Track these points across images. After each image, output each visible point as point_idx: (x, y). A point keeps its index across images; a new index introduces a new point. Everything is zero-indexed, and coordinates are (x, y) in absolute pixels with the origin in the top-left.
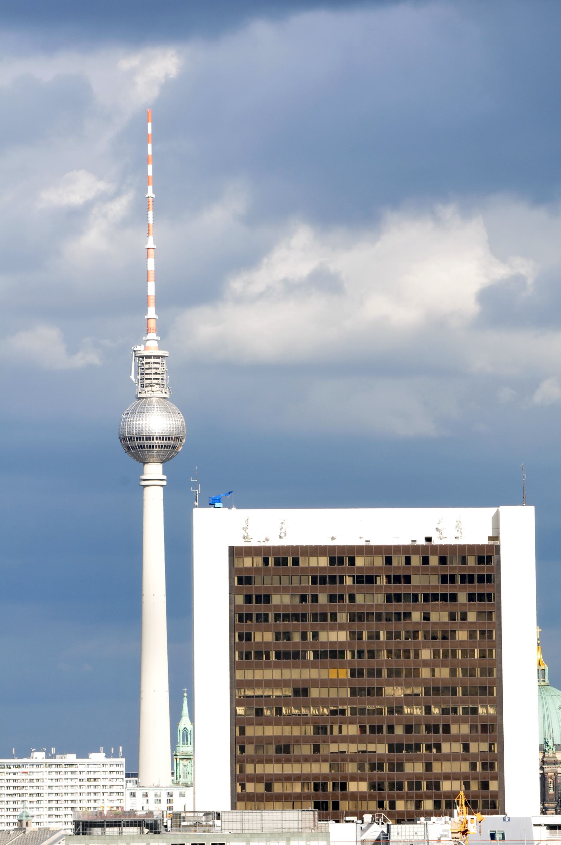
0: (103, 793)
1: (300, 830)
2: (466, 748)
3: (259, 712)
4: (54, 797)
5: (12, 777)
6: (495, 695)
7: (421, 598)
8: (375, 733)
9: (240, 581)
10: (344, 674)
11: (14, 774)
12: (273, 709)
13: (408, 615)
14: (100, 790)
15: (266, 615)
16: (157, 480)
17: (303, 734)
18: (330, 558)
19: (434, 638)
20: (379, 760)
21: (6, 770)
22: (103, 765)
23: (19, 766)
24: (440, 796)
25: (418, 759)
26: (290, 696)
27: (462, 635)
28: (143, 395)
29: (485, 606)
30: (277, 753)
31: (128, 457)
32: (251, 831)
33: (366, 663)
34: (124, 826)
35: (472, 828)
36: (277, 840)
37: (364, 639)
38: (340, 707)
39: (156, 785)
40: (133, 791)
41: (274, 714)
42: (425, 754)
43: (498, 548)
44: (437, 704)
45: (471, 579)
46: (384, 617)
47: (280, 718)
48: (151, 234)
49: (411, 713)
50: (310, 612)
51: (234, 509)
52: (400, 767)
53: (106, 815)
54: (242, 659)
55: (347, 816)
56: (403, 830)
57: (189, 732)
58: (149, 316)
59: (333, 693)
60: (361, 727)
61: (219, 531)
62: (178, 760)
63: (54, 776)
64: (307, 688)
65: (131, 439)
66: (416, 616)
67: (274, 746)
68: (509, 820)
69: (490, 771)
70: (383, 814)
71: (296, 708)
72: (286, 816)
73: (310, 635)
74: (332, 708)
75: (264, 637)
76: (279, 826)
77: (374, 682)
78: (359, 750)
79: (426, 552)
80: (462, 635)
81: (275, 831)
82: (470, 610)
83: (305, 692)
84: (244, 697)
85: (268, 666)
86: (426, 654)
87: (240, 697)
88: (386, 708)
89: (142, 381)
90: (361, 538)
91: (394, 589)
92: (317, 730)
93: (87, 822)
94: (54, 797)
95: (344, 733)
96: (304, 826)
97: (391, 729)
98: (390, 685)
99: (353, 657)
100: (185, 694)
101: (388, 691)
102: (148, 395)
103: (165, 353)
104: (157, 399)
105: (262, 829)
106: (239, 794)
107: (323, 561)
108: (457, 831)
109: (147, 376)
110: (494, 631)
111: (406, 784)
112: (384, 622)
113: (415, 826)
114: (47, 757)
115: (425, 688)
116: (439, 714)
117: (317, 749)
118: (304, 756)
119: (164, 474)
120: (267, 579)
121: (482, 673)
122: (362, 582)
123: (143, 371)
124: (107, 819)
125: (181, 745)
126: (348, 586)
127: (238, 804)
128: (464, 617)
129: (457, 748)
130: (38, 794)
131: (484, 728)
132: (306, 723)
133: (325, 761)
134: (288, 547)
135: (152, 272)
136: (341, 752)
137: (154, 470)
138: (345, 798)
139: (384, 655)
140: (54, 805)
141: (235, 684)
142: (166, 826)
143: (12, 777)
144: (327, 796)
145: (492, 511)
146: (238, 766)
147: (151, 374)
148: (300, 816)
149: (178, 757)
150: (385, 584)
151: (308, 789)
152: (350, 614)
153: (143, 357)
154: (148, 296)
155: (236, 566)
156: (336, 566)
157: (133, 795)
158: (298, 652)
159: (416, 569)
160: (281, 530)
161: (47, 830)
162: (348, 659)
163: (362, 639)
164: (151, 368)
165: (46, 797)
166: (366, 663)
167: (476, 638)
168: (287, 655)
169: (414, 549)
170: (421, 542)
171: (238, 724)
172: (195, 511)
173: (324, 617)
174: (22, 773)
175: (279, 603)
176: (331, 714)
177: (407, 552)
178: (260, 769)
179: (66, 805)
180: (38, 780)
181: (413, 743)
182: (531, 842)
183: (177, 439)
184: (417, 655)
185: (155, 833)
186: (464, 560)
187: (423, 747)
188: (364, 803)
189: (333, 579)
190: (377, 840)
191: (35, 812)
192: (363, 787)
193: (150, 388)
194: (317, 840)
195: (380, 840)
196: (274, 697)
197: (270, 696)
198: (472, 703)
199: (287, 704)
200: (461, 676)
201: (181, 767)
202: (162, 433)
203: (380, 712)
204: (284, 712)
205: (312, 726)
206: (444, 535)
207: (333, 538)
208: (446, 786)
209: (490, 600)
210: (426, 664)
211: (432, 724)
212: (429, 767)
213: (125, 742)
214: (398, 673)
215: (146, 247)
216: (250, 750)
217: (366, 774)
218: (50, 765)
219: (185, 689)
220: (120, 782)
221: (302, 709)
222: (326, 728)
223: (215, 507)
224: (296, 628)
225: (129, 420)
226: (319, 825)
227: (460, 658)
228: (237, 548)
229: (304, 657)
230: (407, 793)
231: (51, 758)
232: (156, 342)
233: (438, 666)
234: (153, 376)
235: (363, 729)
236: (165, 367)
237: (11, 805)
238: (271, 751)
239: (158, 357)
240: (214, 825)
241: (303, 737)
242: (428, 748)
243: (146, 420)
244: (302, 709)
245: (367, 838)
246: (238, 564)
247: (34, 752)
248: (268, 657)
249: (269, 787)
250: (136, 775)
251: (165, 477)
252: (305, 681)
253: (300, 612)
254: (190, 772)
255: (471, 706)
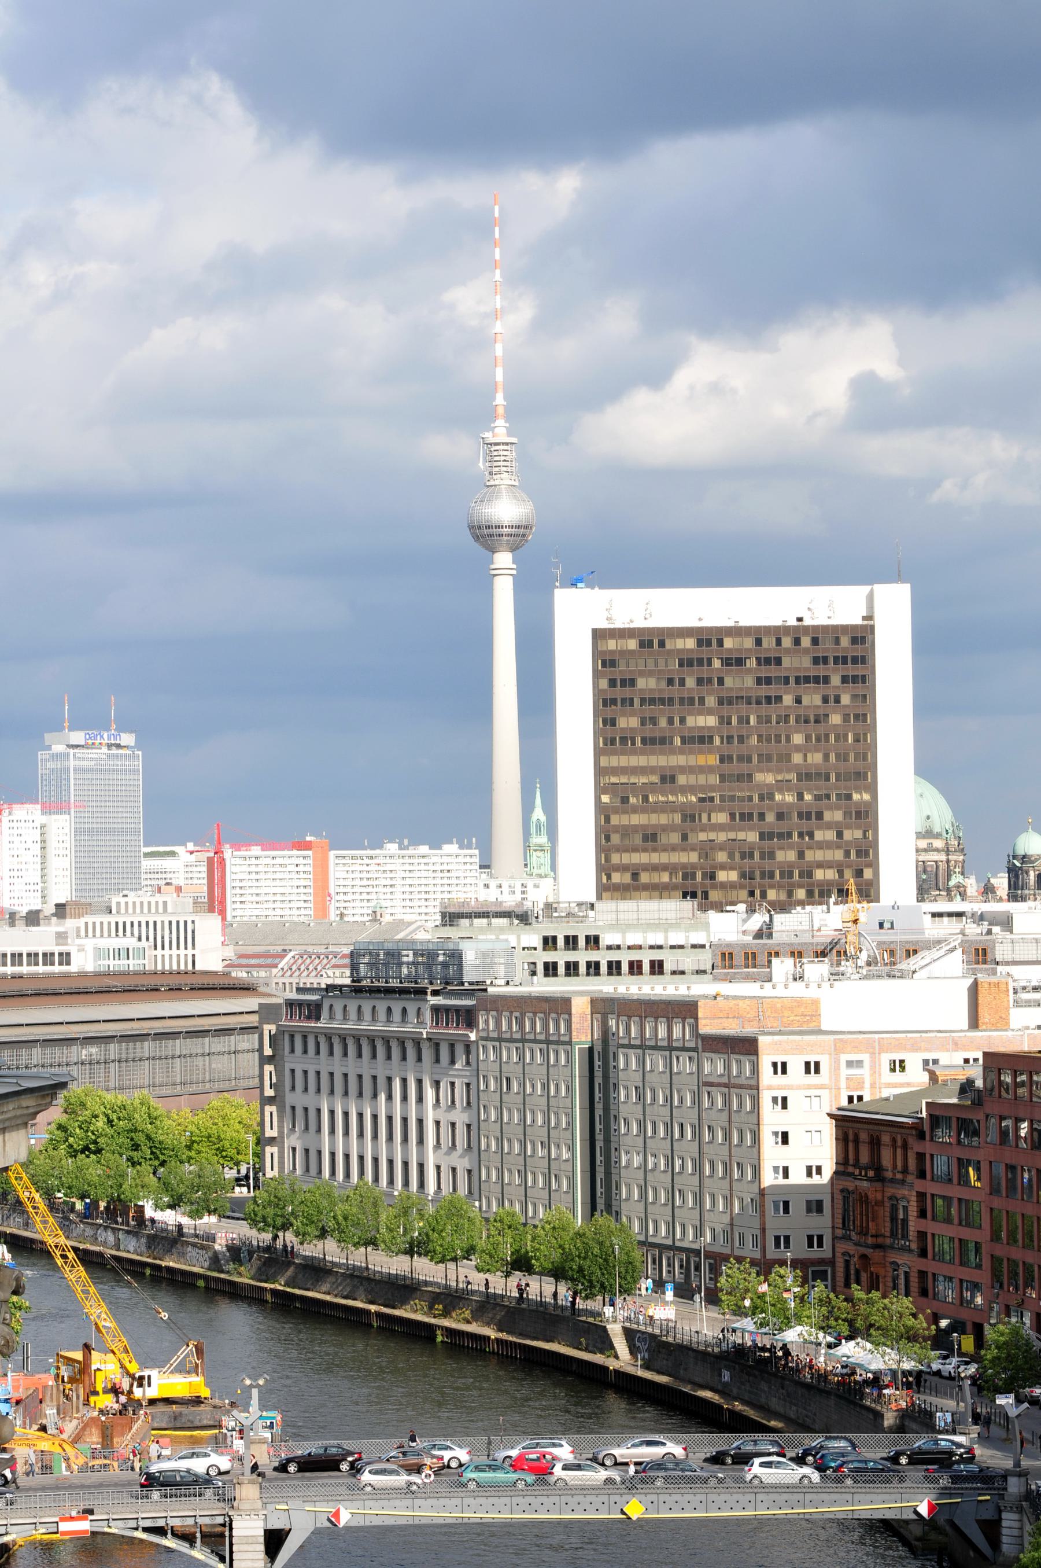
2: (840, 835)
3: (625, 800)
4: (407, 889)
5: (365, 868)
7: (792, 680)
10: (713, 760)
13: (779, 699)
14: (454, 881)
15: (632, 700)
19: (806, 721)
21: (360, 861)
24: (813, 884)
25: (790, 847)
27: (836, 719)
28: (492, 483)
31: (476, 545)
33: (735, 749)
35: (863, 918)
43: (872, 627)
44: (809, 791)
46: (754, 700)
47: (646, 807)
50: (676, 696)
51: (597, 589)
52: (772, 855)
59: (702, 780)
61: (581, 614)
63: (408, 867)
65: (480, 527)
66: (788, 700)
71: (662, 795)
73: (677, 720)
75: (628, 722)
76: (656, 916)
77: (744, 768)
80: (836, 719)
81: (652, 922)
82: (845, 693)
83: (673, 779)
85: (634, 752)
86: (798, 739)
91: (765, 671)
92: (684, 818)
94: (407, 889)
95: (713, 821)
97: (762, 816)
98: (761, 771)
99: (722, 743)
102: (496, 483)
103: (514, 440)
107: (690, 643)
112: (754, 706)
114: (400, 848)
117: (685, 837)
120: (632, 662)
123: (491, 458)
128: (837, 700)
129: (830, 835)
130: (391, 886)
132: (673, 811)
133: (693, 850)
134: (653, 629)
137: (503, 559)
138: (714, 887)
139: (754, 741)
140: (407, 896)
141: (600, 772)
143: (365, 868)
145: (865, 589)
146: (603, 855)
153: (491, 444)
156: (704, 648)
157: (487, 886)
158: (665, 738)
159: (787, 651)
161: (402, 921)
165: (399, 889)
166: (735, 749)
168: (653, 741)
169: (786, 629)
171: (603, 812)
172: (556, 591)
173: (691, 701)
175: (644, 687)
177: (778, 633)
178: (626, 858)
179: (420, 896)
183: (526, 527)
184: (788, 739)
186: (837, 641)
187: (795, 835)
188: (735, 893)
189: (700, 662)
191: (388, 904)
192: (733, 876)
199: (654, 792)
201: (534, 859)
207: (700, 619)
208: (819, 874)
209: (864, 682)
210: (798, 749)
212: (801, 855)
214: (769, 759)
216: (615, 839)
220: (473, 874)
229: (672, 743)
233: (809, 751)
234: (502, 464)
235: (732, 816)
237: (365, 896)
238: (638, 840)
239: (507, 444)
240: (586, 916)
242: (801, 835)
246: (601, 647)
248: (633, 743)
249: (635, 876)
250: (488, 867)
251: (514, 566)
252: (672, 767)
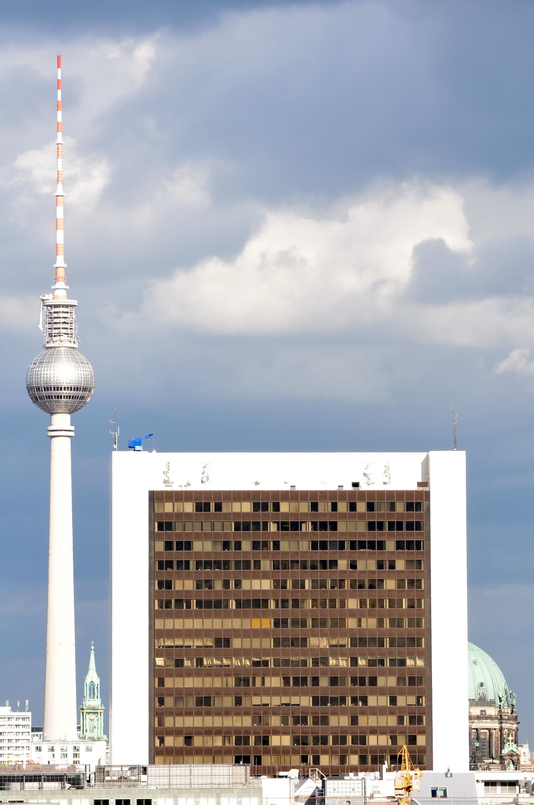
0: (9, 747)
1: (231, 786)
2: (393, 701)
3: (179, 663)
6: (423, 646)
7: (347, 545)
8: (299, 686)
9: (160, 527)
10: (268, 624)
12: (193, 659)
13: (334, 564)
15: (188, 562)
16: (65, 430)
17: (224, 686)
18: (254, 503)
19: (361, 587)
20: (302, 713)
22: (9, 718)
24: (365, 750)
25: (343, 713)
26: (211, 647)
29: (414, 555)
30: (197, 705)
33: (290, 613)
34: (45, 781)
36: (207, 796)
37: (288, 588)
38: (263, 658)
39: (62, 739)
40: (39, 746)
41: (195, 665)
42: (350, 707)
43: (428, 494)
44: (363, 655)
45: (400, 526)
46: (309, 565)
47: (200, 670)
49: (336, 665)
51: (154, 452)
52: (325, 720)
53: (25, 769)
54: (162, 608)
55: (279, 771)
56: (340, 786)
57: (96, 686)
58: (57, 265)
59: (256, 643)
60: (284, 678)
61: (137, 477)
62: (85, 714)
64: (229, 639)
65: (38, 389)
66: (343, 564)
67: (195, 698)
68: (451, 776)
69: (418, 725)
70: (317, 769)
71: (217, 659)
72: (217, 771)
73: (232, 584)
74: (255, 659)
75: (184, 585)
76: (209, 781)
77: (299, 632)
78: (282, 702)
80: (390, 584)
81: (204, 786)
82: (399, 558)
83: (228, 643)
84: (163, 647)
85: (189, 615)
86: (352, 604)
87: (159, 647)
88: (311, 659)
89: (50, 330)
90: (285, 483)
91: (320, 536)
92: (238, 681)
95: (267, 685)
96: (235, 781)
97: (316, 681)
98: (315, 635)
99: (277, 606)
100: (93, 647)
102: (56, 345)
103: (74, 302)
104: (66, 348)
105: (191, 784)
106: (157, 748)
107: (247, 507)
108: (401, 787)
110: (423, 581)
111: (331, 738)
112: (309, 570)
113: (344, 782)
115: (351, 639)
117: (238, 701)
118: (225, 708)
119: (71, 425)
120: (188, 525)
122: (286, 529)
123: (51, 320)
124: (27, 774)
125: (88, 699)
126: (272, 533)
127: (157, 758)
128: (392, 566)
129: (384, 701)
132: (227, 675)
133: (247, 714)
135: (61, 220)
136: (264, 705)
137: (62, 421)
138: (267, 752)
139: (309, 605)
141: (155, 634)
142: (89, 781)
144: (247, 750)
146: (156, 719)
147: (60, 323)
148: (231, 771)
149: (85, 711)
150: (310, 530)
151: (230, 743)
152: (274, 561)
153: (51, 306)
154: (57, 244)
155: (156, 511)
156: (260, 512)
157: (39, 749)
159: (343, 516)
160: (203, 474)
162: (272, 608)
163: (286, 588)
164: (60, 318)
166: (290, 613)
168: (208, 604)
169: (340, 495)
170: (348, 487)
171: (157, 676)
172: (114, 453)
173: (247, 564)
176: (253, 666)
177: (334, 497)
181: (338, 696)
182: (474, 799)
183: (85, 389)
184: (343, 604)
185: (78, 788)
186: (392, 506)
187: (349, 700)
188: (287, 757)
189: (256, 525)
190: (311, 796)
192: (286, 741)
193: (58, 338)
194: (249, 796)
195: (315, 796)
196: (195, 647)
197: (190, 647)
198: (400, 654)
199: (208, 655)
200: (388, 627)
201: (87, 721)
202: (70, 383)
203: (304, 663)
204: (205, 663)
205: (234, 678)
206: (371, 481)
207: (257, 483)
208: (372, 740)
209: (419, 548)
210: (352, 613)
212: (354, 720)
214: (324, 623)
215: (55, 195)
216: (169, 702)
217: (289, 727)
219: (92, 642)
221: (224, 660)
222: (248, 680)
223: (135, 450)
224: (218, 576)
225: (37, 370)
226: (251, 781)
227: (388, 608)
229: (227, 606)
232: (65, 291)
233: (364, 616)
234: (61, 326)
235: (286, 680)
236: (74, 316)
238: (191, 703)
239: (67, 306)
240: (139, 781)
241: (224, 688)
242: (354, 700)
243: (54, 370)
244: (224, 660)
245: (301, 795)
246: (158, 510)
248: (188, 606)
249: (188, 740)
250: (40, 729)
251: (72, 428)
252: (228, 631)
253: (222, 560)
254: (96, 727)
255: (398, 658)
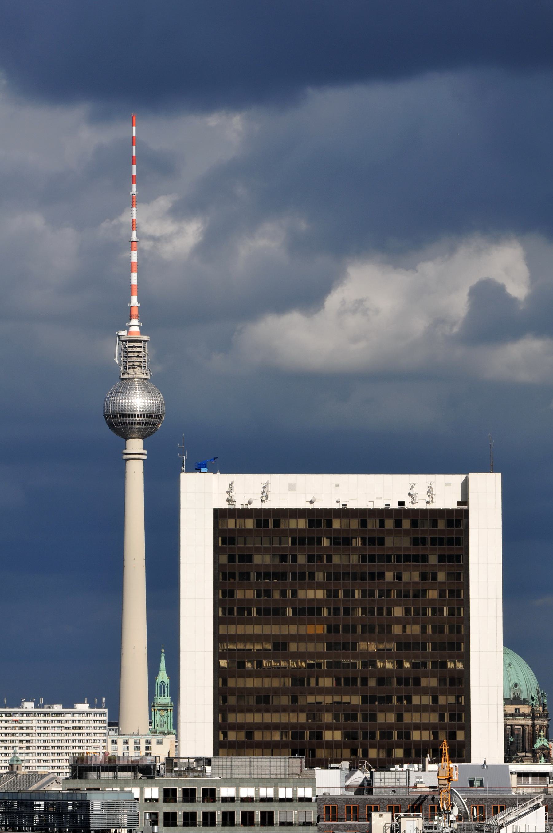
1: (287, 776)
2: (435, 700)
3: (241, 665)
4: (42, 744)
6: (462, 650)
10: (321, 629)
11: (6, 722)
12: (254, 662)
13: (381, 575)
15: (248, 574)
20: (353, 710)
23: (10, 715)
25: (390, 710)
27: (432, 594)
28: (126, 376)
32: (240, 777)
34: (119, 771)
39: (136, 733)
43: (467, 512)
48: (134, 228)
49: (383, 667)
52: (373, 717)
56: (386, 776)
59: (311, 647)
60: (336, 679)
63: (42, 724)
65: (114, 416)
66: (389, 576)
67: (255, 697)
71: (275, 662)
72: (274, 763)
73: (289, 593)
76: (267, 772)
77: (350, 637)
78: (335, 701)
79: (400, 514)
80: (432, 594)
81: (263, 776)
82: (441, 570)
86: (398, 612)
87: (223, 650)
93: (83, 767)
95: (321, 685)
97: (365, 682)
98: (364, 640)
99: (329, 614)
100: (163, 650)
101: (362, 646)
102: (130, 376)
105: (251, 774)
108: (444, 778)
109: (130, 359)
114: (36, 707)
116: (410, 667)
121: (451, 630)
123: (126, 354)
126: (325, 547)
130: (27, 741)
131: (452, 682)
132: (284, 676)
133: (302, 711)
137: (136, 446)
139: (359, 612)
141: (218, 638)
146: (220, 715)
147: (134, 357)
151: (286, 738)
153: (126, 341)
155: (220, 527)
156: (314, 528)
157: (114, 742)
159: (390, 532)
160: (262, 494)
162: (325, 615)
164: (134, 352)
167: (445, 597)
168: (267, 612)
169: (387, 512)
170: (394, 506)
172: (183, 475)
173: (302, 576)
174: (13, 721)
176: (308, 668)
178: (241, 718)
180: (27, 728)
182: (508, 789)
183: (156, 416)
184: (389, 612)
185: (149, 778)
186: (435, 524)
187: (395, 699)
188: (339, 751)
189: (311, 541)
197: (251, 650)
199: (267, 658)
200: (431, 632)
203: (354, 665)
204: (264, 665)
208: (416, 735)
210: (398, 620)
211: (403, 677)
212: (400, 717)
213: (107, 694)
216: (232, 700)
218: (38, 714)
219: (163, 646)
221: (282, 662)
223: (201, 472)
226: (305, 772)
228: (221, 510)
229: (284, 613)
230: (379, 741)
231: (40, 707)
234: (135, 359)
235: (338, 681)
238: (252, 701)
239: (140, 341)
240: (204, 771)
242: (400, 700)
244: (282, 662)
247: (24, 701)
248: (250, 613)
249: (249, 735)
250: (116, 724)
251: (145, 452)
